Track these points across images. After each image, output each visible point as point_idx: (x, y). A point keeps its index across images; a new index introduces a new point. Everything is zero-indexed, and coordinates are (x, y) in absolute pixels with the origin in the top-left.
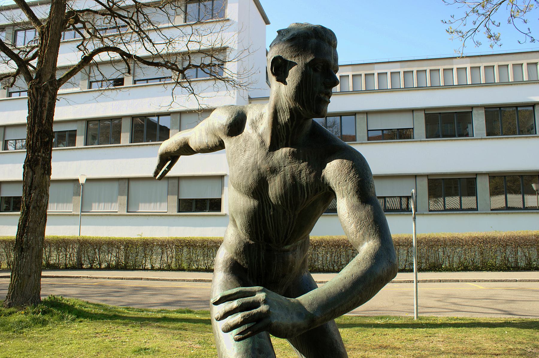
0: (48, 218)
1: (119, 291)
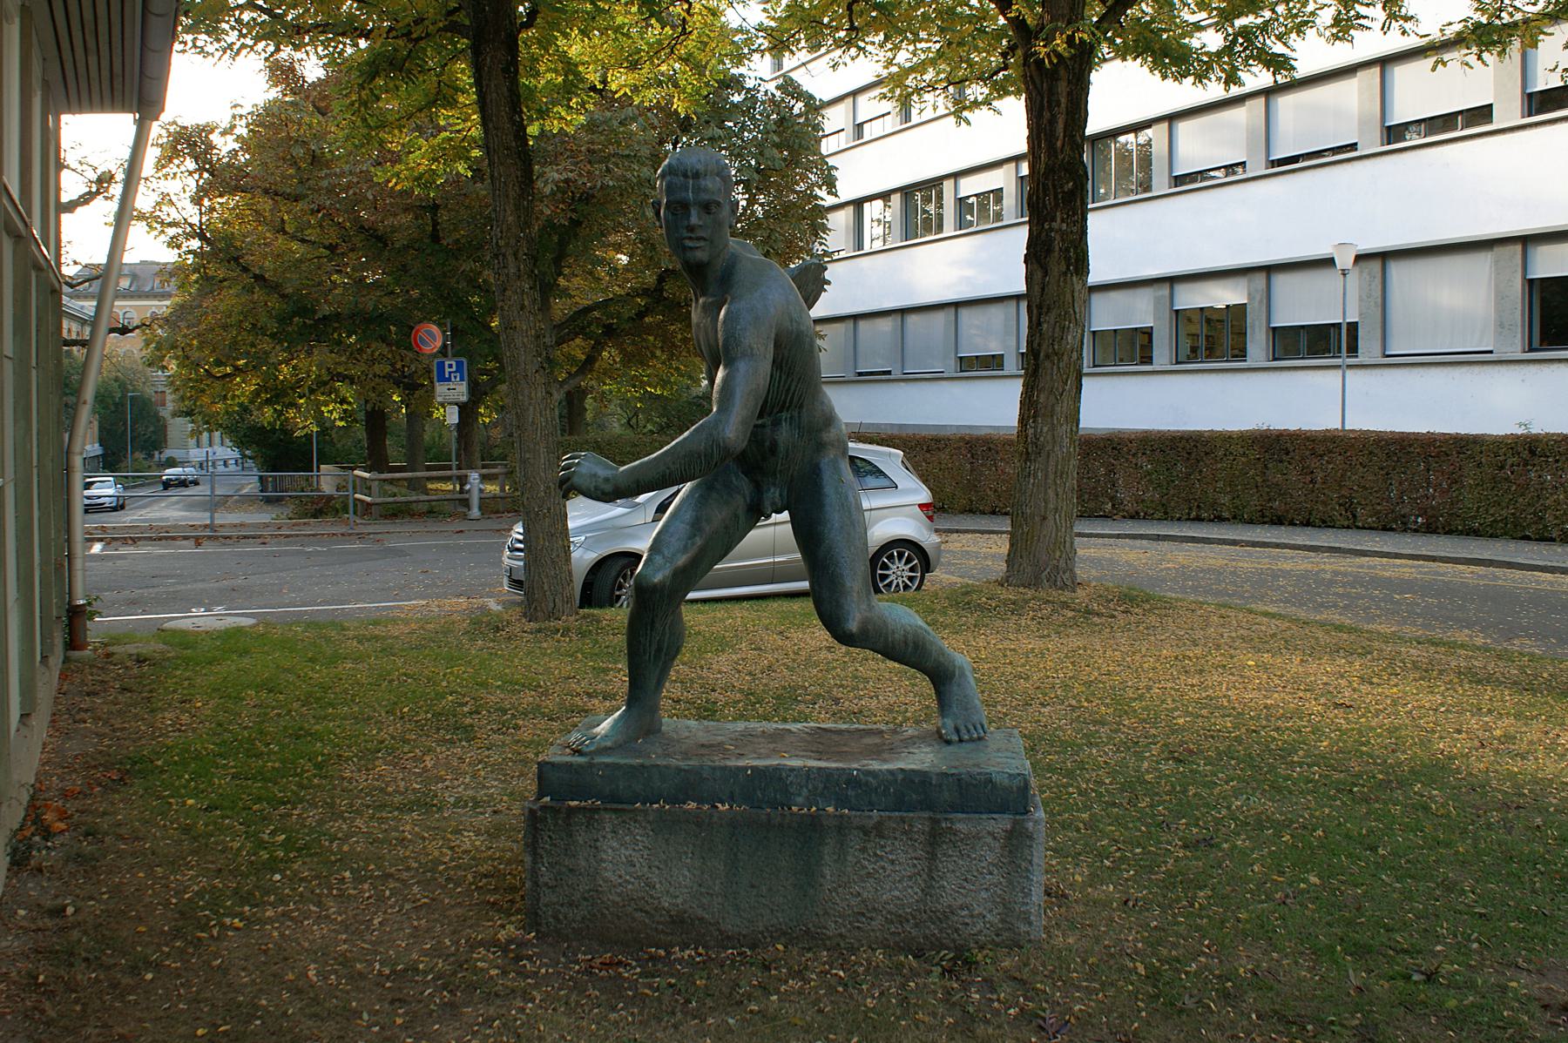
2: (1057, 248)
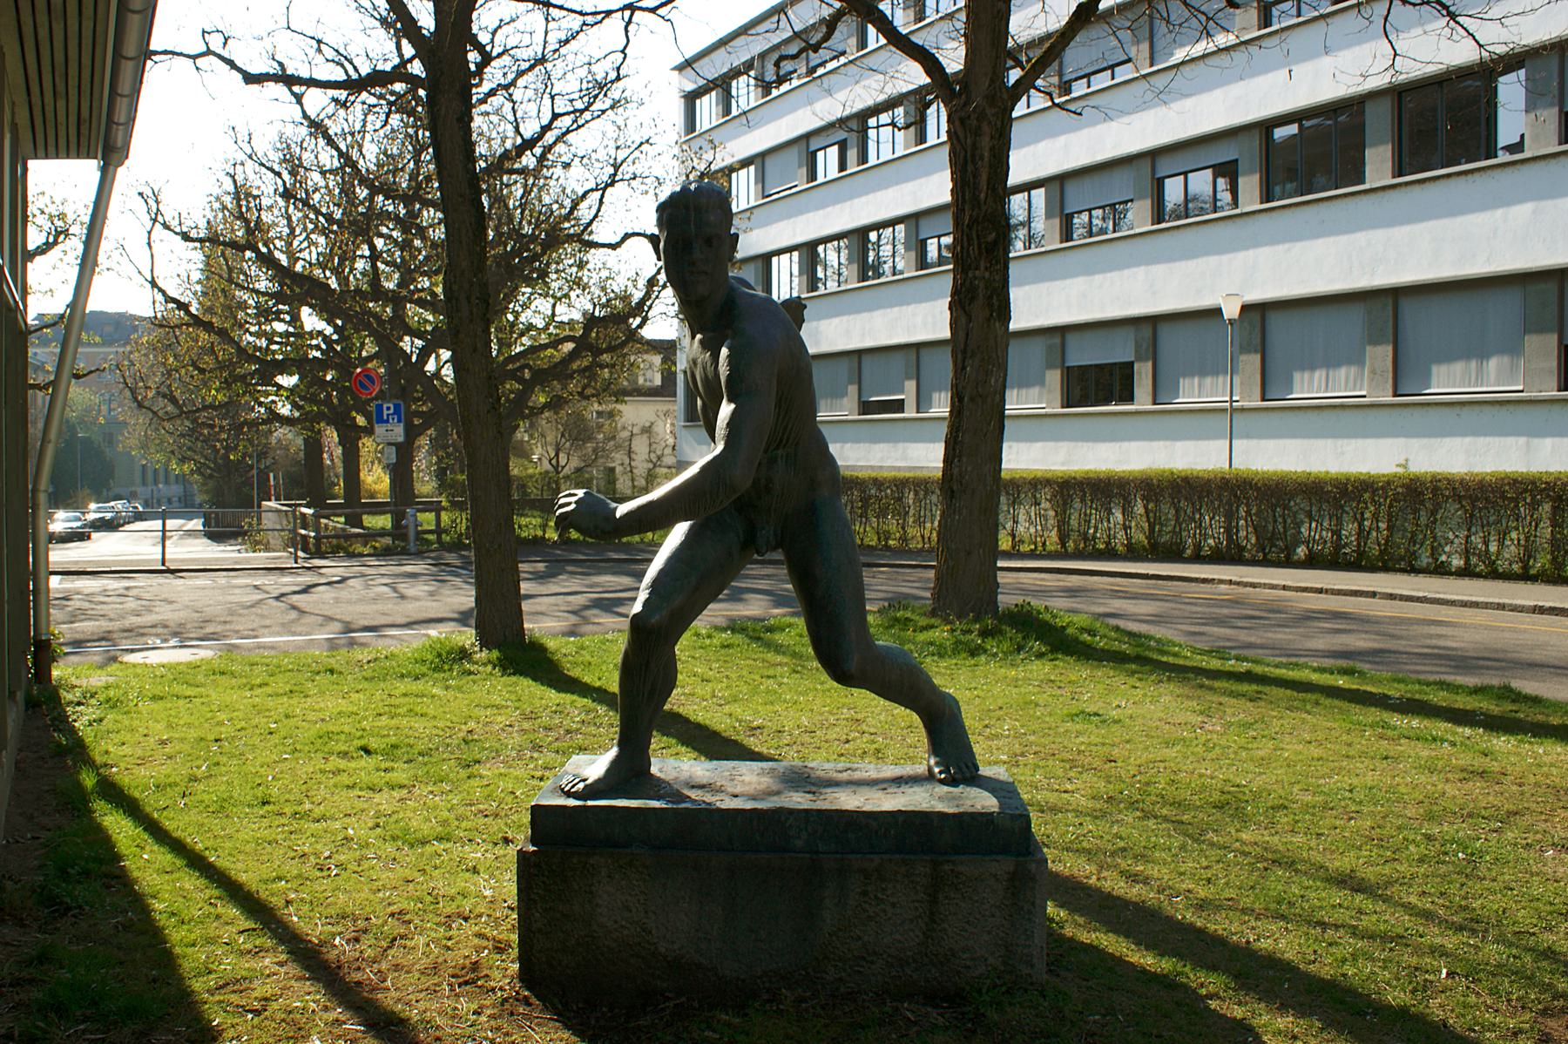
0: (1007, 422)
1: (1273, 614)
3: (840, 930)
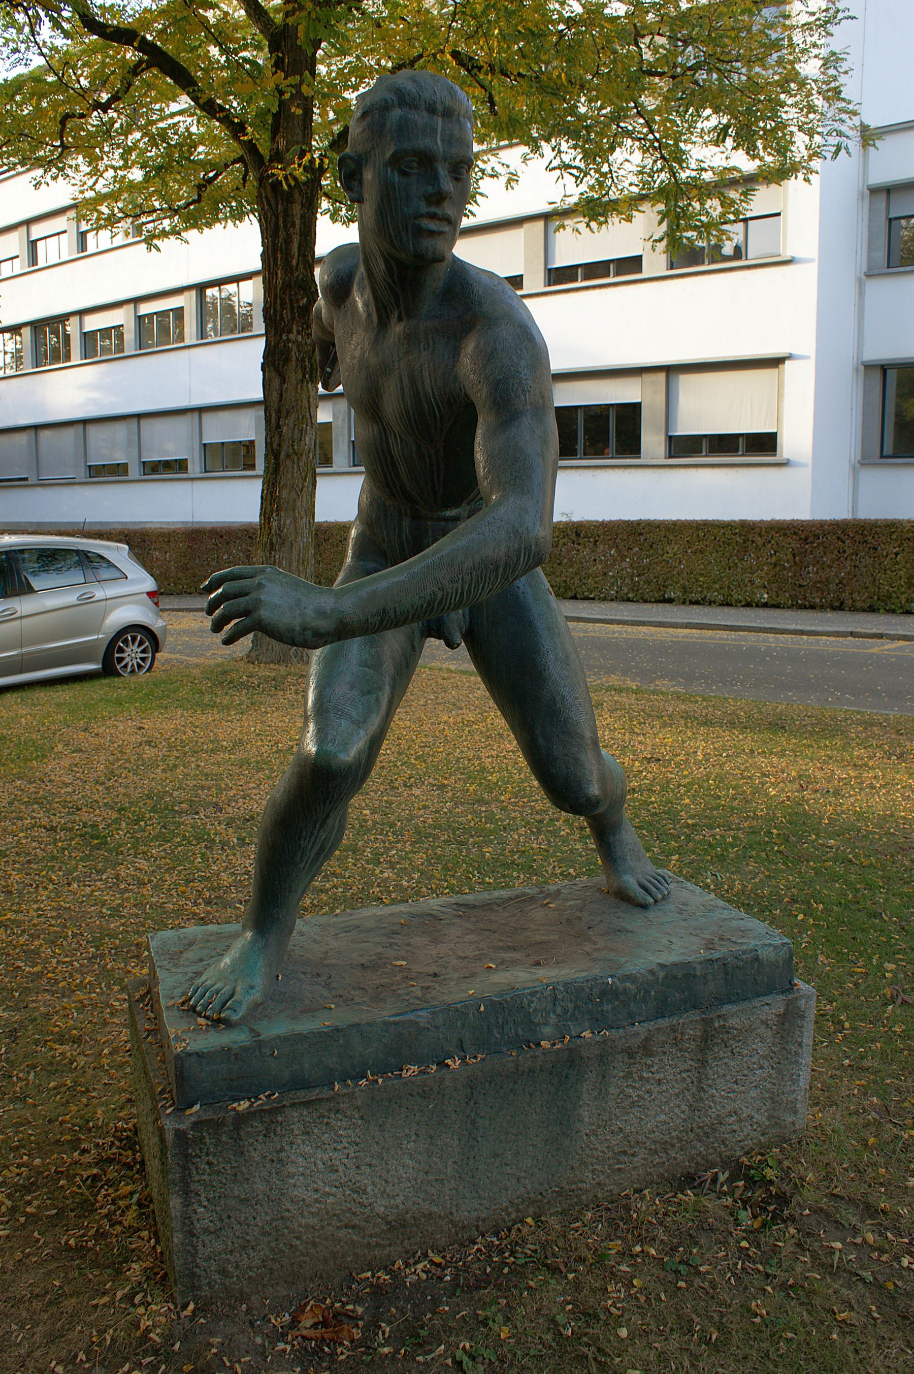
2: (294, 358)
3: (599, 1127)
